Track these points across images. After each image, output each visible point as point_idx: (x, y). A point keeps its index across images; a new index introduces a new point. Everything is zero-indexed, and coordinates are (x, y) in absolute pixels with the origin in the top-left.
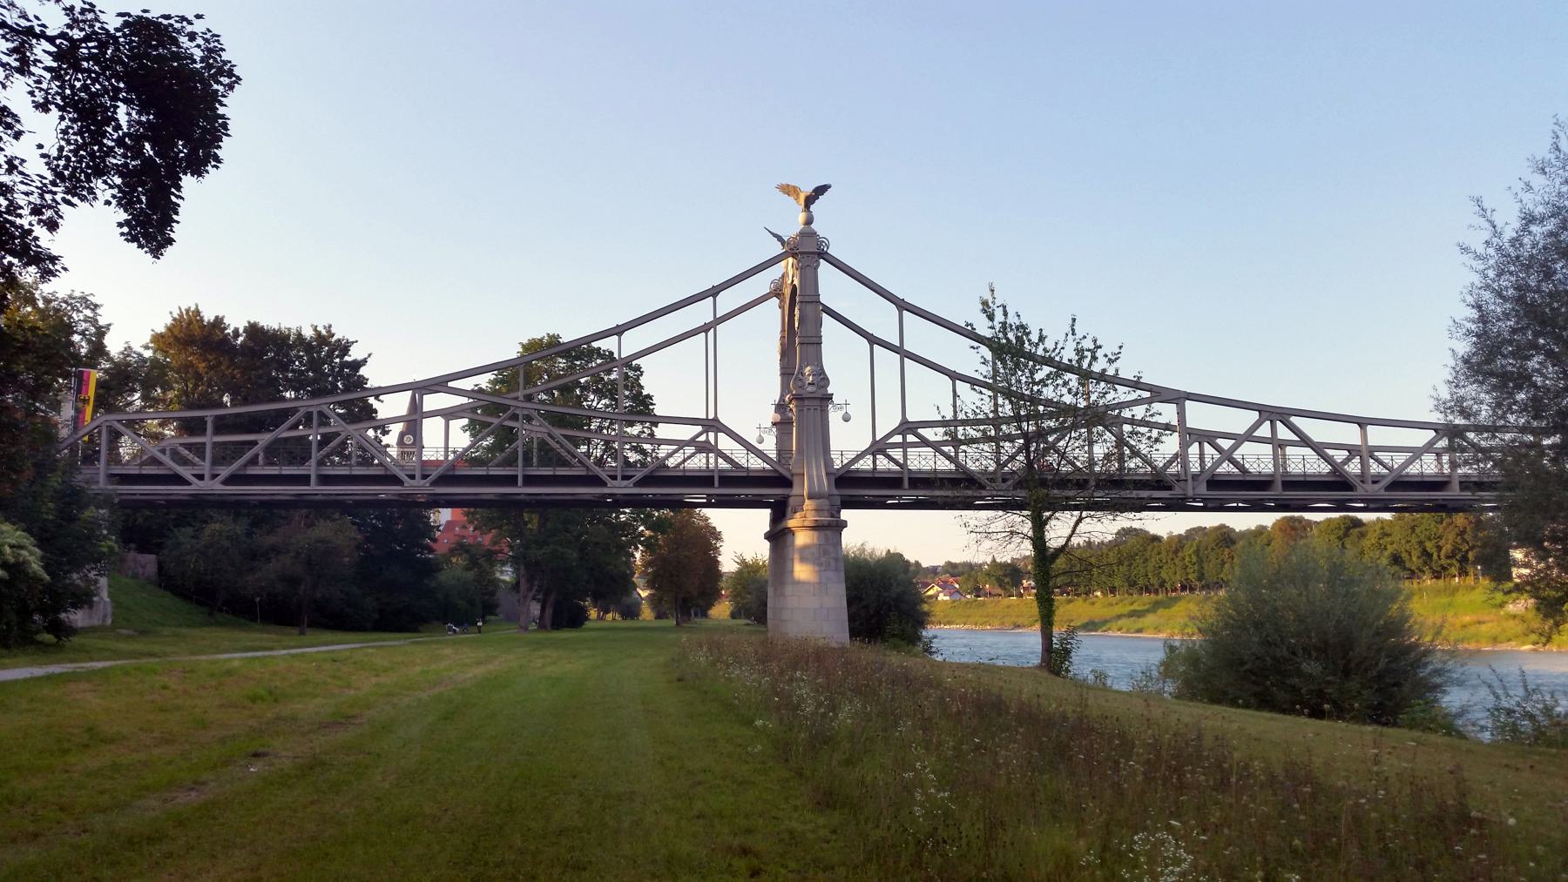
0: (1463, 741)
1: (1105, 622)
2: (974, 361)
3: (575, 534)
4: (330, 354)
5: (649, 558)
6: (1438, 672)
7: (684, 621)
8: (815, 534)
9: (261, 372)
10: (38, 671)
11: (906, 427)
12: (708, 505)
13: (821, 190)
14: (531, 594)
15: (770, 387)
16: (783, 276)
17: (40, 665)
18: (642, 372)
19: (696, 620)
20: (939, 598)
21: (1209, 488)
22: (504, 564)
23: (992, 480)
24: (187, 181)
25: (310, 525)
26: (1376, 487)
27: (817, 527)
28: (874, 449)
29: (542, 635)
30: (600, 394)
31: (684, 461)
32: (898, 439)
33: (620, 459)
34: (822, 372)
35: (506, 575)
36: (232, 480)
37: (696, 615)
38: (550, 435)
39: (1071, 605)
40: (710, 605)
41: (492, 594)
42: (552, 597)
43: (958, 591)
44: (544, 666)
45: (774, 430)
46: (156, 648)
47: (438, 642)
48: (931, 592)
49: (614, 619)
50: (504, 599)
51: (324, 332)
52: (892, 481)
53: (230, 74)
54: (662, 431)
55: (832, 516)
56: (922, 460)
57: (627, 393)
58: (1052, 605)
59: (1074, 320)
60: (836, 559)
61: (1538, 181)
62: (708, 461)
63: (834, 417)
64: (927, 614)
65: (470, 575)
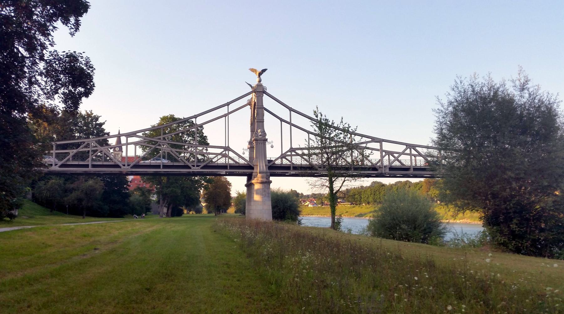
1: (365, 214)
2: (314, 129)
3: (180, 184)
4: (92, 121)
5: (205, 192)
6: (444, 228)
7: (218, 214)
8: (261, 185)
9: (67, 127)
10: (16, 228)
11: (292, 150)
12: (226, 175)
13: (264, 71)
14: (164, 205)
15: (247, 135)
16: (251, 98)
17: (11, 227)
18: (203, 128)
19: (222, 214)
20: (309, 206)
22: (154, 194)
23: (320, 167)
24: (84, 99)
25: (86, 181)
27: (262, 183)
28: (282, 157)
29: (168, 219)
30: (189, 135)
31: (218, 160)
32: (289, 153)
33: (196, 158)
34: (264, 131)
35: (154, 198)
36: (62, 166)
37: (222, 212)
38: (171, 151)
39: (354, 208)
40: (227, 209)
41: (149, 204)
42: (171, 206)
43: (315, 204)
44: (171, 228)
45: (248, 150)
46: (45, 222)
47: (133, 221)
48: (306, 204)
49: (193, 214)
50: (154, 207)
51: (89, 113)
52: (287, 168)
53: (92, 67)
54: (210, 150)
55: (267, 179)
56: (297, 161)
57: (198, 135)
58: (335, 208)
59: (342, 118)
60: (268, 193)
61: (452, 93)
62: (226, 160)
63: (268, 146)
64: (300, 211)
65: (141, 198)
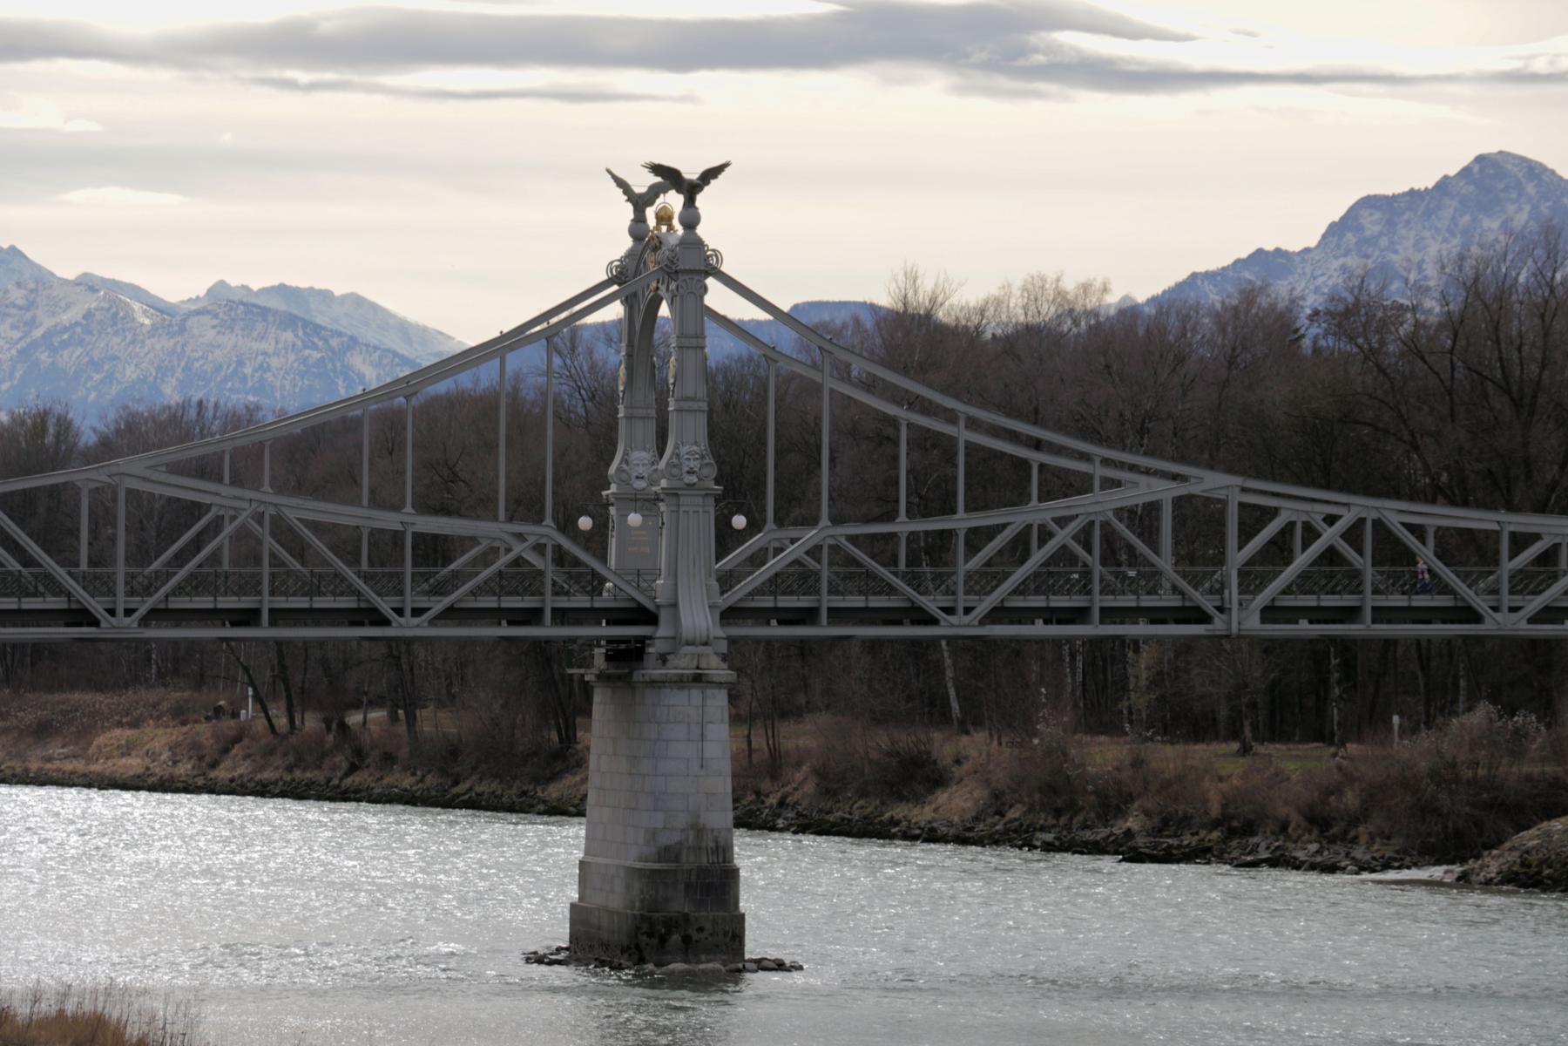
0: (796, 975)
21: (1264, 620)
26: (1514, 616)
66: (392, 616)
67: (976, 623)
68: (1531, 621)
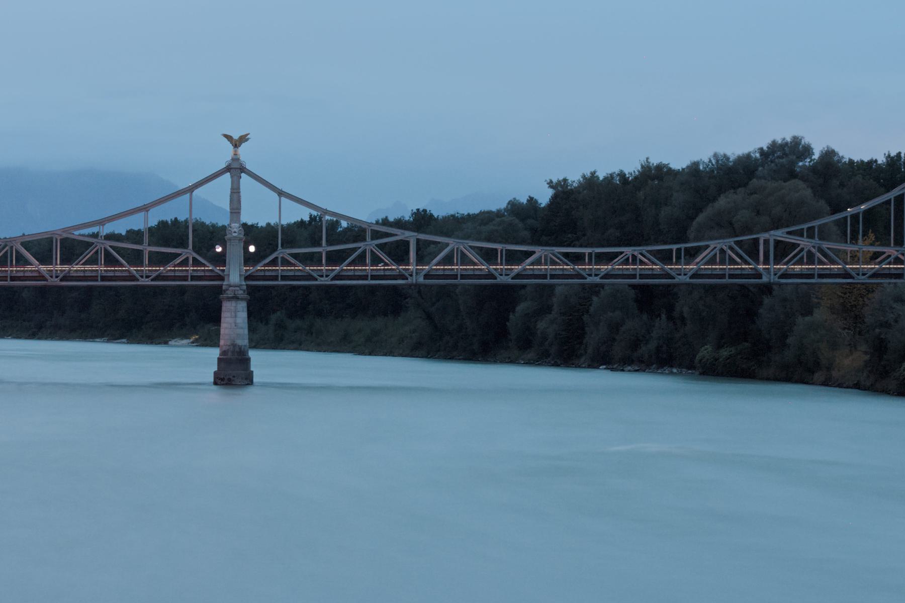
21: (424, 279)
26: (685, 277)
66: (140, 278)
67: (329, 280)
68: (512, 279)
